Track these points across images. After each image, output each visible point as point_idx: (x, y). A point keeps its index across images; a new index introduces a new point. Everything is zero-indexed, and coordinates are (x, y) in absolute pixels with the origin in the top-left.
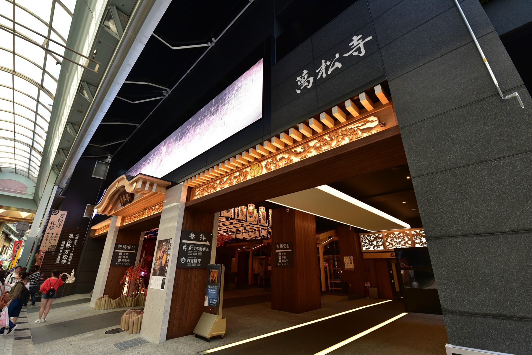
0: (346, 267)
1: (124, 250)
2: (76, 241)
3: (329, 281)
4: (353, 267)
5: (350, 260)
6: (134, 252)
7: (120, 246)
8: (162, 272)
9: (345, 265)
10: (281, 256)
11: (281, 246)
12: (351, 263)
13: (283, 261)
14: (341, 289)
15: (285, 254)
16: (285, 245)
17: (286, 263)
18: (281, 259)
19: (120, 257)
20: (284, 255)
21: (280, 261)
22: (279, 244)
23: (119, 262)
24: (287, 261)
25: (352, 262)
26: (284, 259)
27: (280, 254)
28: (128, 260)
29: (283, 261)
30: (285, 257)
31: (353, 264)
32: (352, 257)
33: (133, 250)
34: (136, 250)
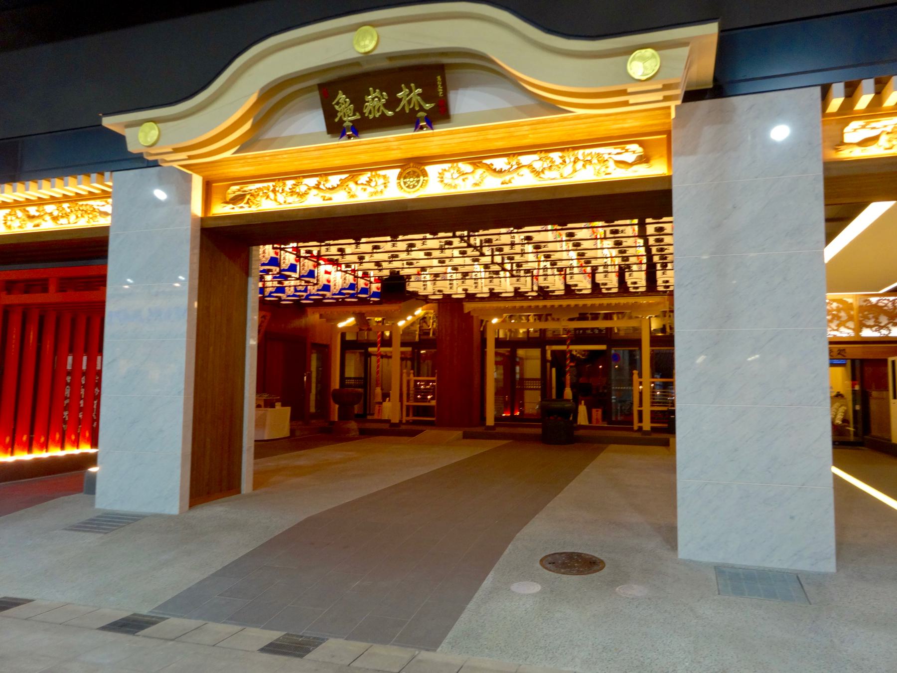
3: (405, 403)
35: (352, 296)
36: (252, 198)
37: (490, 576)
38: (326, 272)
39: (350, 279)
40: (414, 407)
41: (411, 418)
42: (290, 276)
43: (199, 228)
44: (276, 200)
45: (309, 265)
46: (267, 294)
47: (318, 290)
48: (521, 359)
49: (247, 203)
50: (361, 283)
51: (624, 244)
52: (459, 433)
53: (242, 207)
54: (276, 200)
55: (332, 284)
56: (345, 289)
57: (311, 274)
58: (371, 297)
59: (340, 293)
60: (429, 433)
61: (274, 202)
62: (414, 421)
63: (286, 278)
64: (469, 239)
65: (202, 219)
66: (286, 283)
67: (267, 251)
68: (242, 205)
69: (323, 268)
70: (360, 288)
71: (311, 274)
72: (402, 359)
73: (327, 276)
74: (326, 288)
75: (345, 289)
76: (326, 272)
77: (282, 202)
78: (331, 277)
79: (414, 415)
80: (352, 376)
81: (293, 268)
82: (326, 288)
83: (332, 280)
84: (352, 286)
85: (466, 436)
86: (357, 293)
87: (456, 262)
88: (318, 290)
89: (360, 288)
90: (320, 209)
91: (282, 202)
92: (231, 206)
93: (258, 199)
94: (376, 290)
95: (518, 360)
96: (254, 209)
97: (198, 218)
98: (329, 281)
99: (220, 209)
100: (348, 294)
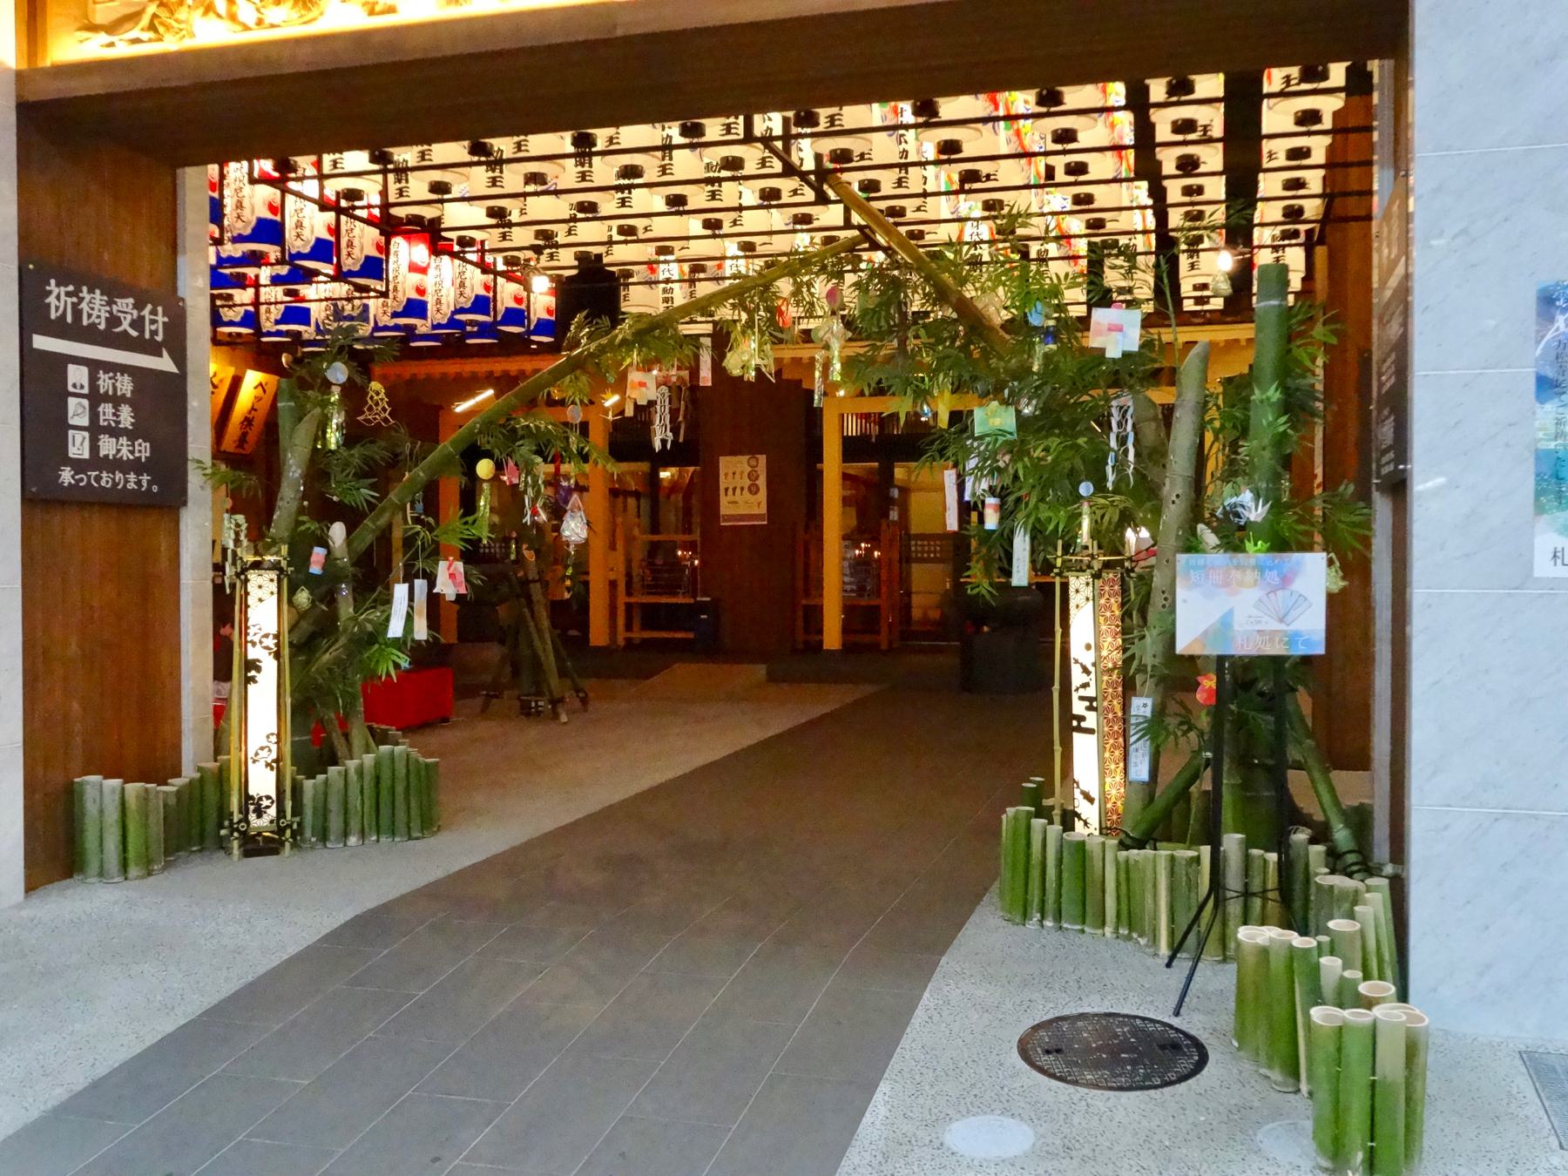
0: (726, 508)
1: (89, 335)
2: (1315, 180)
3: (622, 599)
4: (763, 510)
5: (753, 476)
6: (165, 363)
7: (58, 299)
8: (890, 625)
9: (724, 500)
10: (95, 398)
11: (95, 307)
12: (754, 490)
13: (108, 446)
14: (691, 635)
15: (125, 385)
16: (125, 304)
17: (136, 466)
18: (95, 430)
19: (77, 411)
20: (117, 401)
21: (79, 446)
22: (76, 278)
23: (79, 466)
24: (143, 450)
25: (762, 482)
26: (115, 432)
27: (77, 376)
28: (143, 450)
29: (108, 446)
30: (126, 417)
31: (763, 495)
32: (763, 459)
33: (153, 349)
34: (175, 342)
35: (484, 330)
36: (163, 13)
37: (878, 1096)
38: (415, 268)
39: (476, 281)
40: (643, 606)
41: (638, 635)
42: (317, 273)
43: (13, 104)
44: (233, 17)
45: (362, 239)
46: (267, 326)
47: (395, 315)
48: (905, 491)
49: (152, 27)
50: (507, 292)
51: (1110, 227)
52: (761, 670)
53: (137, 41)
54: (233, 17)
55: (430, 299)
56: (462, 311)
57: (374, 267)
58: (530, 333)
59: (452, 323)
60: (683, 673)
61: (227, 24)
62: (644, 641)
63: (308, 276)
64: (787, 149)
65: (19, 76)
66: (307, 291)
67: (245, 190)
68: (136, 33)
69: (406, 252)
70: (501, 309)
71: (374, 267)
72: (614, 493)
73: (416, 278)
74: (416, 308)
75: (462, 311)
76: (415, 268)
77: (251, 23)
78: (429, 281)
79: (644, 627)
80: (1025, 583)
81: (323, 250)
82: (416, 308)
83: (430, 290)
84: (481, 304)
85: (772, 678)
86: (495, 323)
87: (753, 221)
88: (395, 315)
89: (501, 309)
90: (360, 39)
91: (251, 23)
92: (103, 37)
93: (182, 14)
94: (545, 316)
95: (895, 493)
96: (170, 44)
97: (9, 69)
98: (421, 291)
99: (70, 47)
100: (472, 323)
